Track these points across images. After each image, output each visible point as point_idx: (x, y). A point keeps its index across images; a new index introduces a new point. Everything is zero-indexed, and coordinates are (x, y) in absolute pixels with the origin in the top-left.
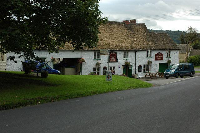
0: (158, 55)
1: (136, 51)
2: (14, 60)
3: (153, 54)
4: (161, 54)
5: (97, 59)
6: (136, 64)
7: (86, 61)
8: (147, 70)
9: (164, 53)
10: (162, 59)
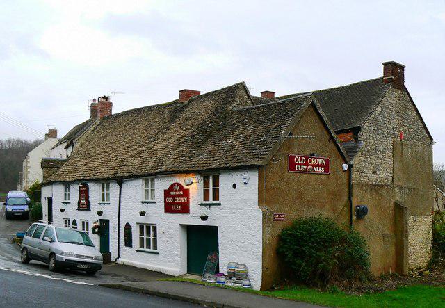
0: (172, 193)
1: (120, 181)
2: (56, 137)
3: (162, 185)
4: (181, 187)
5: (211, 201)
6: (119, 221)
7: (178, 226)
8: (148, 246)
9: (195, 187)
10: (185, 209)
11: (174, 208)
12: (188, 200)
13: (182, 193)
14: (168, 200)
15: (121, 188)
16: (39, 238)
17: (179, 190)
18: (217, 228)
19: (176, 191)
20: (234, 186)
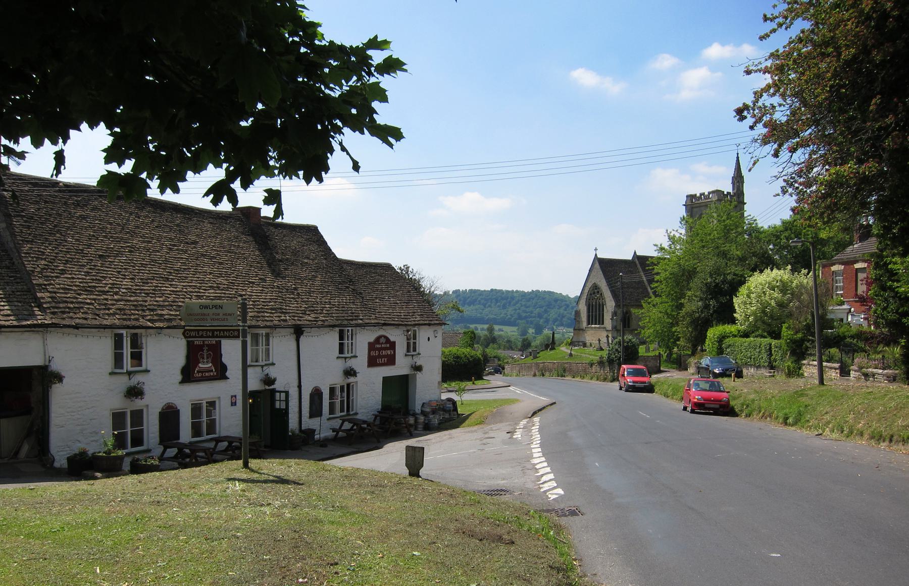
0: (378, 346)
10: (391, 361)
11: (379, 361)
12: (395, 352)
13: (388, 345)
14: (373, 353)
15: (44, 345)
16: (207, 403)
17: (386, 343)
18: (383, 377)
19: (382, 343)
20: (429, 339)
